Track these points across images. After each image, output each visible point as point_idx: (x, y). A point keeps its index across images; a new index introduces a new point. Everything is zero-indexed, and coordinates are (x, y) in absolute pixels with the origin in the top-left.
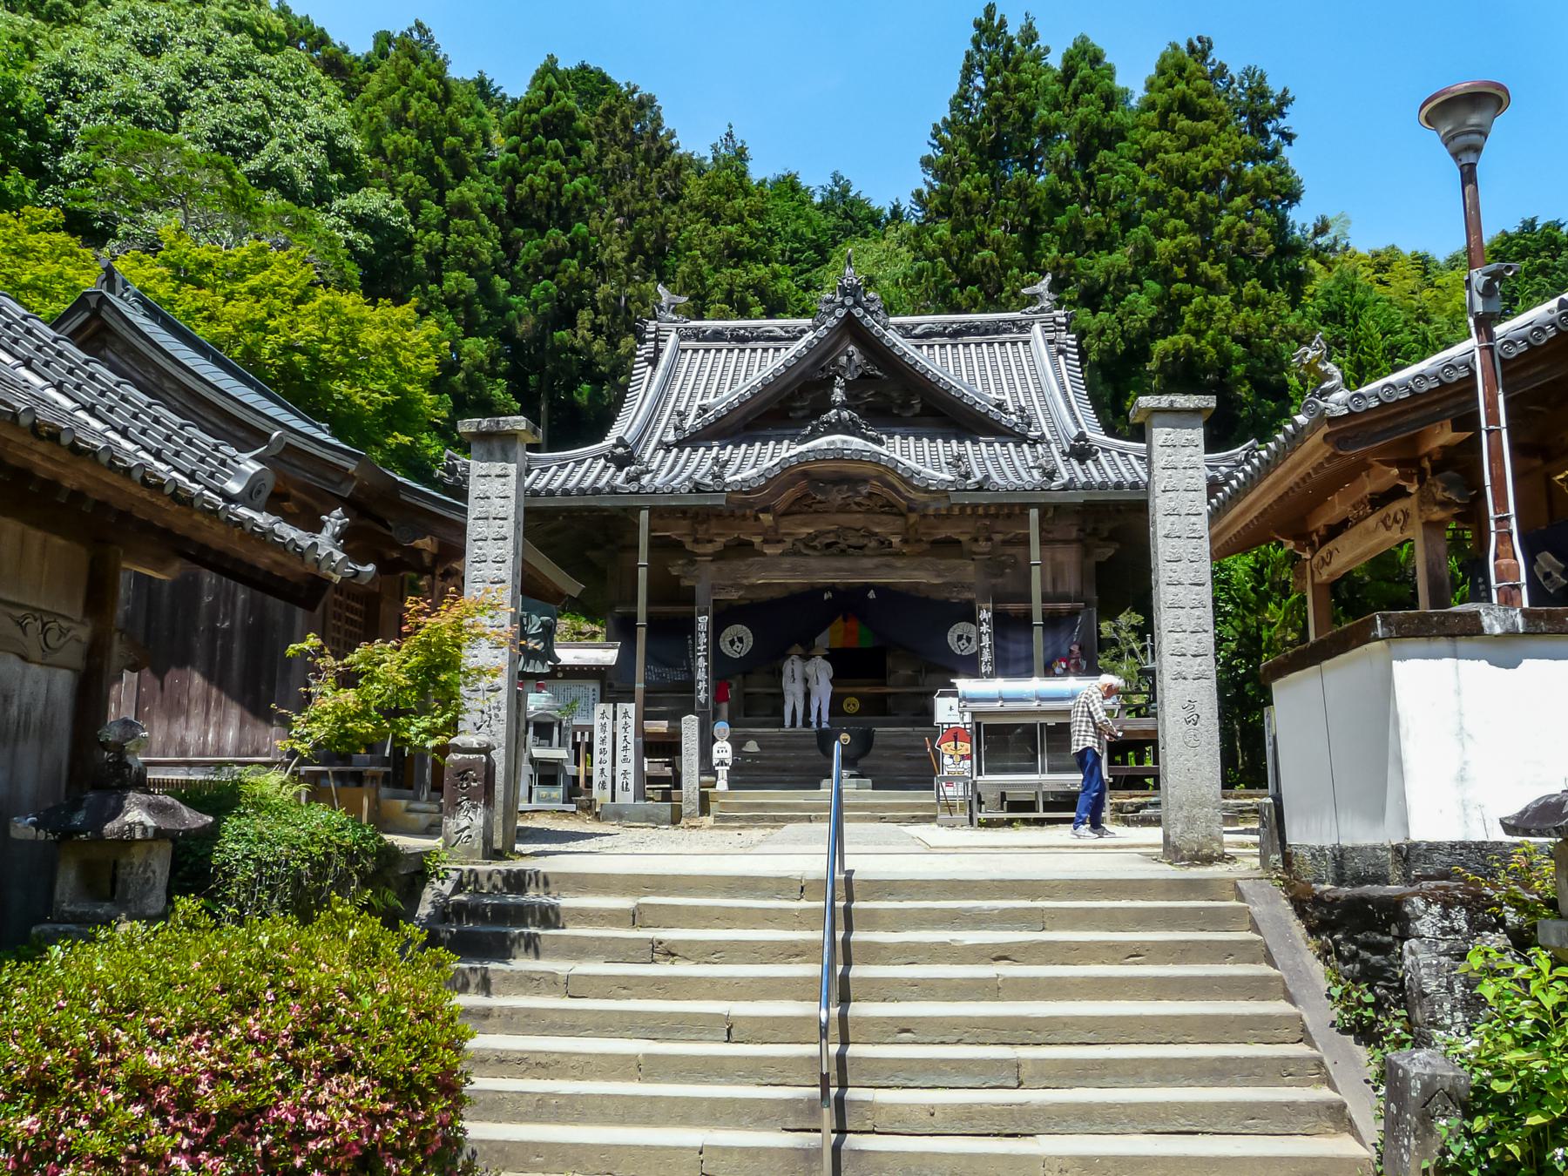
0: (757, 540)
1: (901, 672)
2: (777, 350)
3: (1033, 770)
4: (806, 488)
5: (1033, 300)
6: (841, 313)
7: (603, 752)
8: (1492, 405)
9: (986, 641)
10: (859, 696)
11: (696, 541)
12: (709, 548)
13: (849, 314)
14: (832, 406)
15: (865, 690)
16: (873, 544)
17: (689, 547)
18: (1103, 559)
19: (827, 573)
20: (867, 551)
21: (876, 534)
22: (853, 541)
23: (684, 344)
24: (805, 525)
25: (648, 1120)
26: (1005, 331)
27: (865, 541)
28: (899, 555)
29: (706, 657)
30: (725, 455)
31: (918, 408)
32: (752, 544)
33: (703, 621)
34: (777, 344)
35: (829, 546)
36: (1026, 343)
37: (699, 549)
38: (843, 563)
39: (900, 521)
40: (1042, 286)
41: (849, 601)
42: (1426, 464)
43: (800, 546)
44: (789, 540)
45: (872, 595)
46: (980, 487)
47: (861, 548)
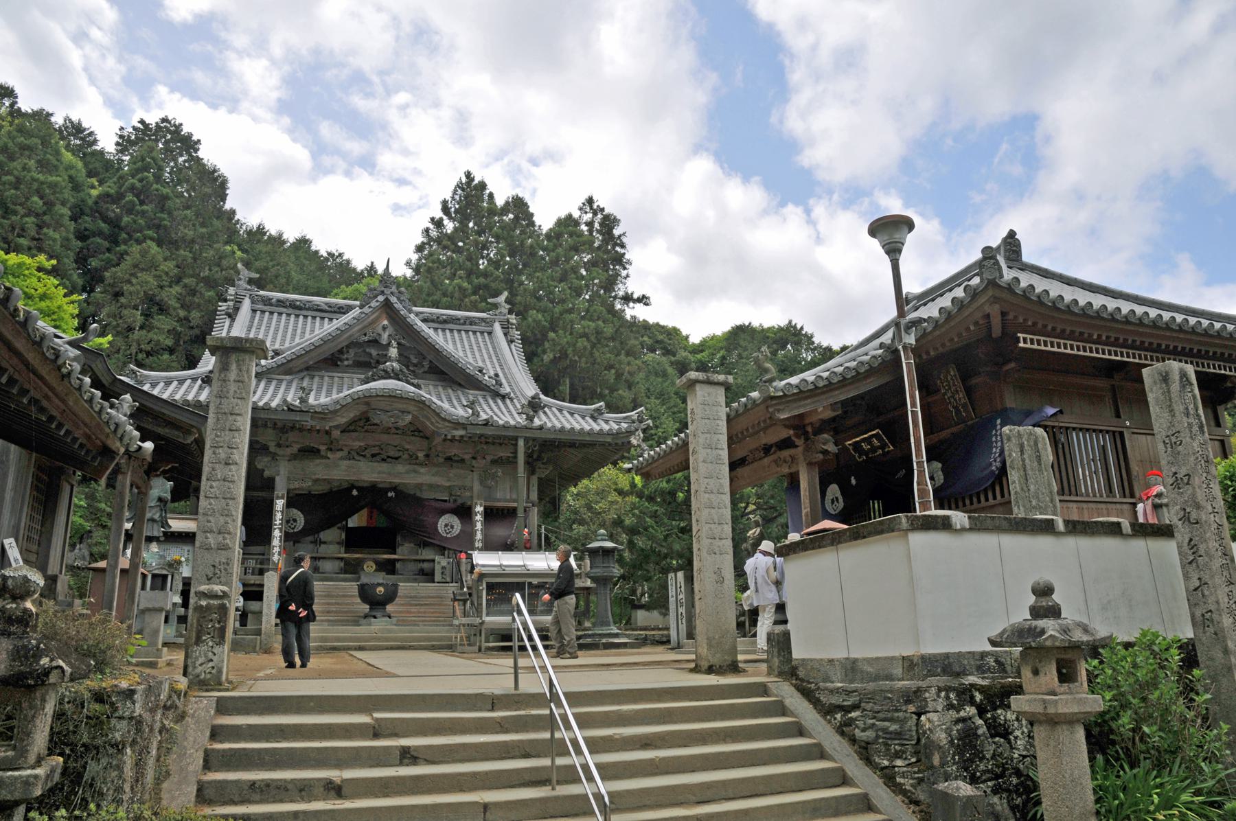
0: (323, 448)
2: (331, 320)
4: (363, 417)
5: (496, 306)
6: (381, 298)
8: (913, 397)
11: (279, 445)
12: (289, 451)
13: (387, 300)
14: (390, 359)
15: (386, 556)
16: (406, 456)
17: (272, 449)
19: (369, 473)
22: (392, 454)
26: (475, 324)
28: (421, 464)
29: (281, 530)
30: (305, 384)
31: (427, 367)
32: (319, 451)
34: (323, 315)
35: (373, 456)
36: (490, 333)
37: (280, 452)
39: (425, 443)
41: (372, 495)
42: (809, 429)
45: (355, 493)
47: (396, 459)
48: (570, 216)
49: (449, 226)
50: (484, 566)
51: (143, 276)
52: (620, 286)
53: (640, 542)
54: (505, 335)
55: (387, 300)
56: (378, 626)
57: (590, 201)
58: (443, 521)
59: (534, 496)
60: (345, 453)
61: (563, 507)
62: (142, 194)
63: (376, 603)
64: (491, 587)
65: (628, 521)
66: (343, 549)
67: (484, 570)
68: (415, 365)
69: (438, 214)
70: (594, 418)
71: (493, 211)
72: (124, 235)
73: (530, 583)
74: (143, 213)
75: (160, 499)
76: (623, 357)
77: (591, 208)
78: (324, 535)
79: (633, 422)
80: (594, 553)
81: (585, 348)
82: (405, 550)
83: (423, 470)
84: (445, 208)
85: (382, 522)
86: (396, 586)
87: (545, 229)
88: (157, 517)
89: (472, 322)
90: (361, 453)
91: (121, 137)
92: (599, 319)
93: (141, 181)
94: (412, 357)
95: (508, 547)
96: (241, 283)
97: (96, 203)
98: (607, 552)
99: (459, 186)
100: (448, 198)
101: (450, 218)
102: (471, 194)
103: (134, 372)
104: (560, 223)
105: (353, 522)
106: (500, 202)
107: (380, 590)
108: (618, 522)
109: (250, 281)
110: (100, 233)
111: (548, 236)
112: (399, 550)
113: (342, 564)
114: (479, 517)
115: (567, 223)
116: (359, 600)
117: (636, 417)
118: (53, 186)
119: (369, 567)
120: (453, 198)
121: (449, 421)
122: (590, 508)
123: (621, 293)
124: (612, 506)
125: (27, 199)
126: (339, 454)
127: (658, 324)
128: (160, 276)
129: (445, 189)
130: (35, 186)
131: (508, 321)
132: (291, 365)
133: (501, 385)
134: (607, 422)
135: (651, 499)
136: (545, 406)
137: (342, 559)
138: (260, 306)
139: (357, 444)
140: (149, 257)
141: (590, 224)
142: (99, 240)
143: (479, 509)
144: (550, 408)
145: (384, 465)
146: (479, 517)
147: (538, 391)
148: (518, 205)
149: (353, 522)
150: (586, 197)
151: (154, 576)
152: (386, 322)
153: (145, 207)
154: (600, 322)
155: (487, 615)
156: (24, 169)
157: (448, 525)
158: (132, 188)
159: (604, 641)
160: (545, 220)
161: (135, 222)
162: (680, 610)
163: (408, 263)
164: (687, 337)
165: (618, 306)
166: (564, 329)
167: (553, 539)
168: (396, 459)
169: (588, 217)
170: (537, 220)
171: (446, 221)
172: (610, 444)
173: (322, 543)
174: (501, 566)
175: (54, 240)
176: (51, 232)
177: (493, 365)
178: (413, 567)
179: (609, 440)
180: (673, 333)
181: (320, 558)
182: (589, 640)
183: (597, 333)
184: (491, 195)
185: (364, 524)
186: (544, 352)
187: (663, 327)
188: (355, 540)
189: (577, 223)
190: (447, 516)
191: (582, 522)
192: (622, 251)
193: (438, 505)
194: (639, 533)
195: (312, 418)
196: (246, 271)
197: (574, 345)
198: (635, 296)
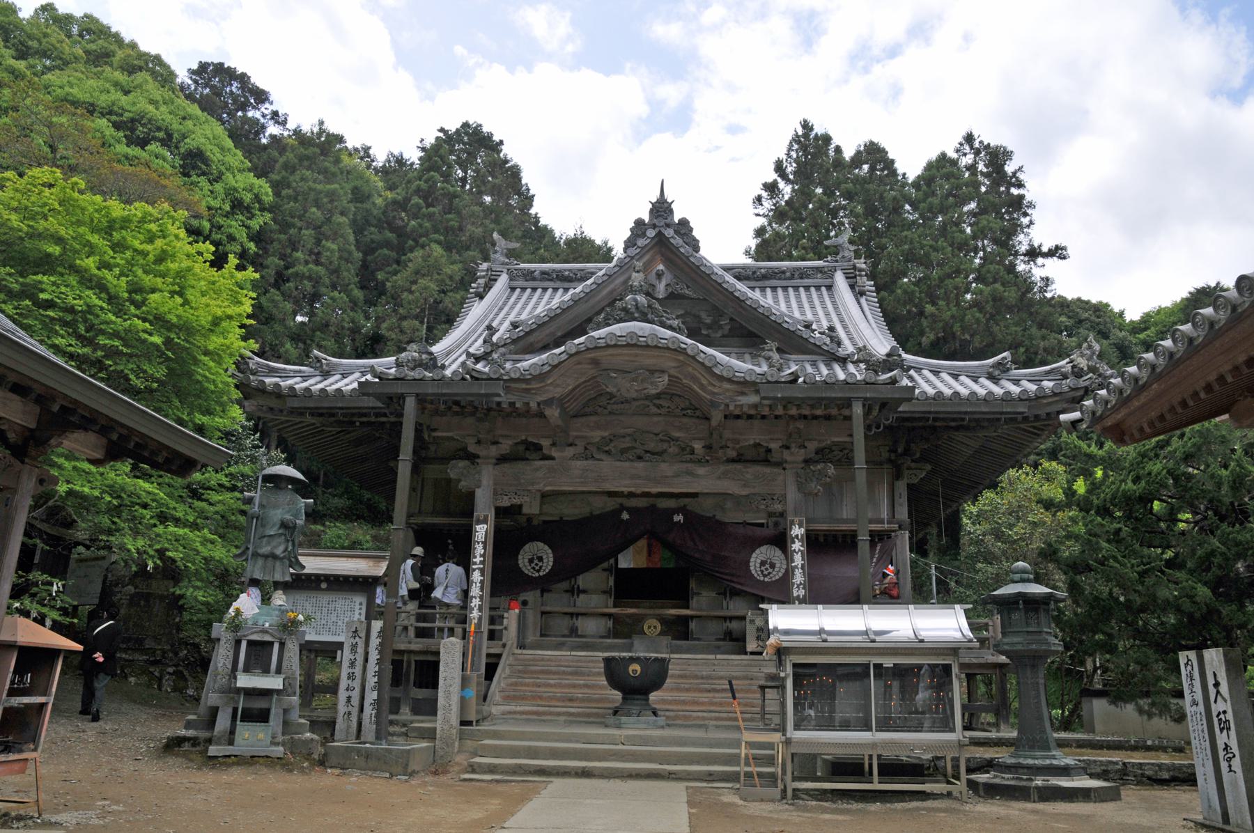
0: (545, 443)
5: (836, 250)
9: (798, 560)
12: (494, 451)
13: (660, 234)
15: (673, 612)
16: (673, 449)
18: (916, 481)
19: (621, 477)
21: (677, 440)
22: (651, 446)
23: (515, 283)
26: (808, 276)
27: (665, 446)
29: (482, 571)
32: (538, 448)
33: (481, 532)
35: (623, 451)
36: (829, 288)
41: (648, 519)
43: (593, 450)
45: (625, 516)
47: (660, 454)
48: (943, 155)
49: (786, 190)
50: (787, 632)
51: (423, 282)
52: (1021, 237)
53: (1095, 585)
54: (852, 287)
55: (660, 234)
56: (634, 730)
57: (969, 138)
59: (903, 513)
60: (580, 449)
61: (964, 540)
62: (428, 196)
63: (635, 689)
64: (802, 673)
65: (1070, 550)
66: (611, 602)
67: (786, 641)
68: (709, 327)
69: (772, 176)
70: (993, 378)
71: (839, 161)
72: (411, 242)
73: (878, 667)
74: (430, 216)
75: (283, 525)
76: (1034, 330)
77: (972, 148)
78: (583, 581)
79: (1065, 377)
80: (1008, 605)
81: (978, 321)
82: (702, 601)
83: (701, 471)
84: (779, 168)
85: (664, 560)
86: (663, 663)
87: (911, 177)
88: (279, 551)
89: (803, 274)
91: (423, 149)
92: (995, 281)
93: (426, 182)
94: (703, 315)
95: (854, 598)
96: (497, 256)
97: (384, 213)
98: (1032, 603)
99: (796, 139)
100: (783, 157)
101: (787, 181)
102: (811, 150)
103: (318, 360)
104: (930, 166)
106: (848, 154)
107: (635, 668)
108: (1050, 553)
109: (511, 254)
110: (387, 244)
111: (916, 184)
112: (694, 602)
113: (610, 624)
114: (797, 546)
115: (941, 167)
116: (603, 681)
117: (1069, 368)
118: (332, 196)
119: (652, 626)
120: (788, 155)
121: (730, 380)
122: (998, 535)
123: (1024, 248)
124: (1040, 525)
125: (306, 211)
126: (570, 452)
127: (1079, 299)
128: (443, 281)
129: (777, 144)
130: (312, 196)
131: (854, 267)
132: (531, 339)
133: (839, 344)
134: (1016, 382)
135: (1104, 511)
136: (910, 368)
137: (609, 615)
138: (521, 283)
139: (597, 435)
140: (432, 260)
141: (972, 168)
142: (385, 251)
143: (797, 531)
144: (918, 370)
145: (640, 465)
146: (797, 546)
147: (895, 343)
148: (874, 153)
149: (626, 561)
150: (964, 133)
151: (250, 643)
152: (661, 267)
153: (431, 209)
154: (998, 286)
155: (797, 727)
156: (302, 179)
158: (418, 191)
159: (1039, 782)
160: (910, 166)
161: (421, 226)
162: (1221, 739)
163: (747, 253)
164: (1121, 314)
165: (1021, 267)
166: (947, 298)
167: (953, 584)
168: (660, 454)
169: (968, 159)
170: (900, 167)
171: (781, 184)
172: (1026, 419)
173: (581, 591)
174: (821, 631)
175: (332, 252)
176: (329, 244)
177: (828, 315)
178: (715, 628)
179: (1022, 409)
180: (1100, 309)
181: (578, 615)
182: (1007, 779)
183: (994, 300)
184: (838, 150)
186: (922, 333)
187: (1088, 302)
188: (630, 587)
189: (954, 163)
190: (764, 549)
191: (989, 558)
192: (1021, 191)
193: (750, 531)
194: (1089, 568)
195: (508, 390)
196: (503, 242)
197: (962, 320)
198: (1045, 249)
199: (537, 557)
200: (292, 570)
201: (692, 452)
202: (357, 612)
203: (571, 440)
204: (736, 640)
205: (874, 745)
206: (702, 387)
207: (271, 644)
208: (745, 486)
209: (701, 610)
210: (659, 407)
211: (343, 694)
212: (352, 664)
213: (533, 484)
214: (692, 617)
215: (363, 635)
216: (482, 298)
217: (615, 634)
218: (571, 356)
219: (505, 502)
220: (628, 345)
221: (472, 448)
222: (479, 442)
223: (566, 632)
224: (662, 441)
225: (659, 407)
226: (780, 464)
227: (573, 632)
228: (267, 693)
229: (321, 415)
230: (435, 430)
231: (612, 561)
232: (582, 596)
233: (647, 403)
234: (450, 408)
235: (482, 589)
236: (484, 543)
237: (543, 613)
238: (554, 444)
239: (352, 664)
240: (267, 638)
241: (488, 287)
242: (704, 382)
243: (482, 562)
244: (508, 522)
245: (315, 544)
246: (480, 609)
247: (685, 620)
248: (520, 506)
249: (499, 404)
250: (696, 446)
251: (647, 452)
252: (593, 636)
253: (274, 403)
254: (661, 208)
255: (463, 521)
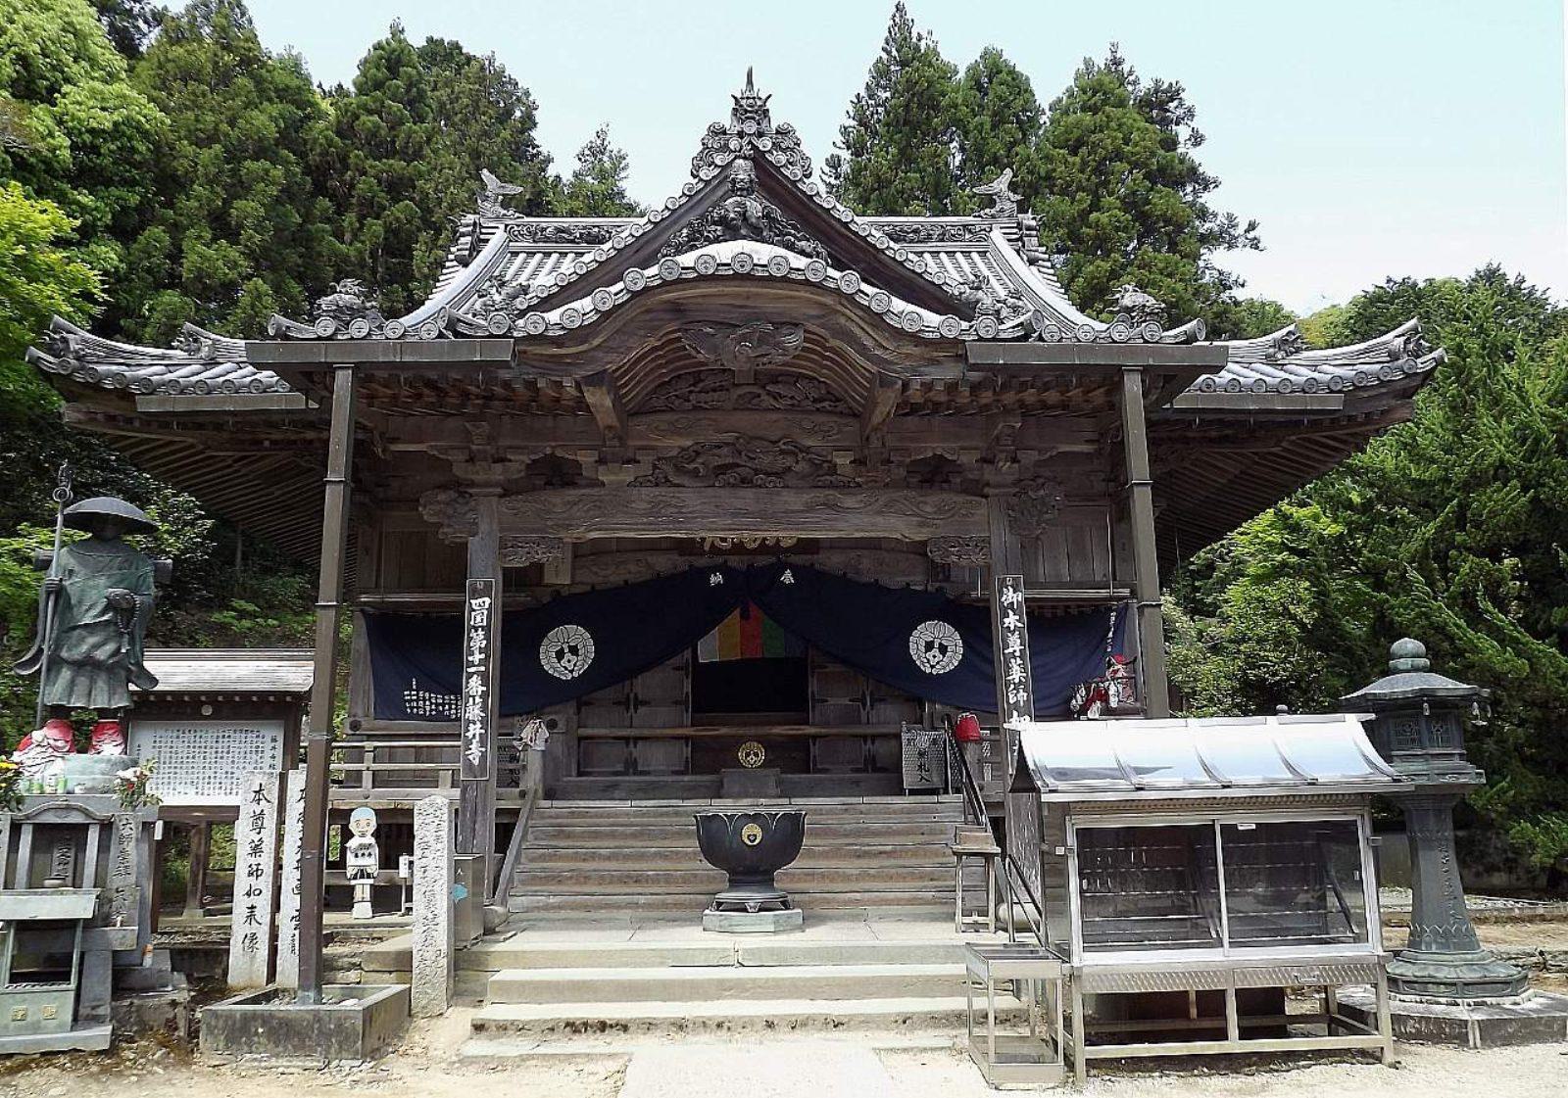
0: (586, 458)
1: (832, 701)
3: (1199, 934)
7: (255, 872)
10: (768, 744)
12: (497, 472)
15: (777, 730)
16: (802, 467)
19: (718, 521)
20: (790, 479)
21: (807, 450)
22: (766, 461)
24: (677, 432)
25: (610, 954)
27: (789, 461)
28: (845, 487)
29: (485, 678)
33: (480, 610)
35: (722, 469)
38: (747, 497)
39: (852, 427)
40: (1001, 184)
43: (669, 469)
44: (646, 459)
45: (788, 577)
46: (1027, 332)
58: (926, 632)
60: (645, 468)
66: (687, 718)
70: (1270, 359)
73: (1229, 831)
83: (850, 502)
86: (794, 822)
90: (682, 468)
105: (710, 649)
107: (752, 833)
116: (694, 845)
119: (753, 756)
126: (628, 473)
131: (1019, 226)
137: (686, 738)
139: (675, 443)
145: (749, 494)
149: (710, 649)
157: (936, 646)
173: (639, 703)
185: (735, 656)
188: (720, 693)
199: (568, 653)
200: (132, 687)
201: (833, 469)
202: (268, 753)
203: (630, 454)
204: (883, 770)
205: (1231, 971)
206: (863, 350)
207: (85, 828)
208: (921, 525)
209: (827, 724)
210: (776, 396)
211: (240, 903)
212: (256, 850)
213: (568, 527)
214: (815, 737)
215: (274, 797)
216: (466, 265)
217: (693, 766)
218: (635, 295)
219: (518, 562)
220: (737, 276)
221: (460, 471)
222: (471, 460)
223: (620, 767)
224: (782, 452)
225: (776, 396)
226: (976, 489)
227: (631, 766)
228: (68, 925)
229: (200, 426)
230: (395, 440)
231: (688, 654)
232: (642, 710)
233: (755, 390)
234: (419, 396)
235: (484, 708)
236: (487, 629)
237: (580, 739)
238: (601, 461)
239: (256, 850)
240: (76, 818)
241: (475, 249)
242: (869, 343)
243: (484, 662)
244: (522, 598)
245: (174, 638)
246: (483, 743)
247: (803, 742)
248: (539, 567)
249: (507, 385)
250: (838, 461)
251: (757, 472)
252: (663, 773)
253: (115, 408)
254: (751, 109)
255: (451, 597)
